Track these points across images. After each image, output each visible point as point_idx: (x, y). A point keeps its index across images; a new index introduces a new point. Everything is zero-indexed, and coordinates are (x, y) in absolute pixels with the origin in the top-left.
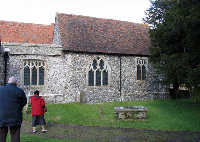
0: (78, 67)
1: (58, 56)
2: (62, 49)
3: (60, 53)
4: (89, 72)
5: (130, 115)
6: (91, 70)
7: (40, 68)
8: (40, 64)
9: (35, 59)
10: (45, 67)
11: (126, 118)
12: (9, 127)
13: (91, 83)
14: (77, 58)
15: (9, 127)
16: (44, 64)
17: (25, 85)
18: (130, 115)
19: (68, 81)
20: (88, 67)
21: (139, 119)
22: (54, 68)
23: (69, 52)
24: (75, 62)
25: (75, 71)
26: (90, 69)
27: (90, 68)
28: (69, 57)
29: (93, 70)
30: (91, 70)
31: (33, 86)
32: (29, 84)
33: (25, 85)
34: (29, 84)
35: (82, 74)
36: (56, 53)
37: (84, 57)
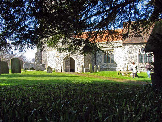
0: (132, 52)
1: (121, 47)
2: (122, 43)
3: (121, 45)
4: (139, 55)
5: (127, 74)
6: (140, 54)
7: (111, 54)
8: (111, 51)
9: (108, 49)
10: (114, 53)
11: (125, 75)
12: (84, 72)
13: (105, 61)
14: (131, 47)
15: (84, 72)
16: (113, 52)
17: (104, 62)
18: (127, 74)
19: (126, 60)
20: (138, 52)
21: (130, 76)
22: (118, 53)
23: (17, 76)
24: (130, 50)
25: (130, 55)
26: (140, 53)
27: (140, 53)
28: (127, 47)
29: (142, 53)
30: (140, 54)
31: (108, 63)
32: (110, 62)
33: (104, 62)
34: (110, 62)
35: (135, 56)
36: (119, 45)
37: (135, 46)
